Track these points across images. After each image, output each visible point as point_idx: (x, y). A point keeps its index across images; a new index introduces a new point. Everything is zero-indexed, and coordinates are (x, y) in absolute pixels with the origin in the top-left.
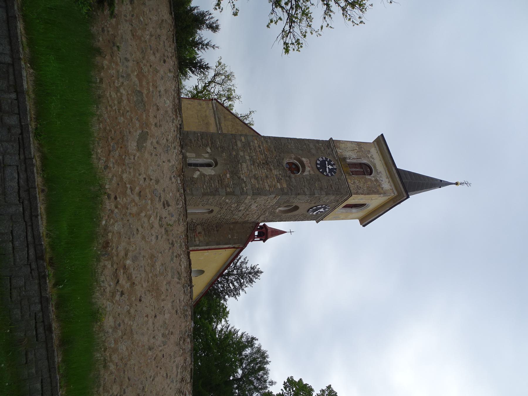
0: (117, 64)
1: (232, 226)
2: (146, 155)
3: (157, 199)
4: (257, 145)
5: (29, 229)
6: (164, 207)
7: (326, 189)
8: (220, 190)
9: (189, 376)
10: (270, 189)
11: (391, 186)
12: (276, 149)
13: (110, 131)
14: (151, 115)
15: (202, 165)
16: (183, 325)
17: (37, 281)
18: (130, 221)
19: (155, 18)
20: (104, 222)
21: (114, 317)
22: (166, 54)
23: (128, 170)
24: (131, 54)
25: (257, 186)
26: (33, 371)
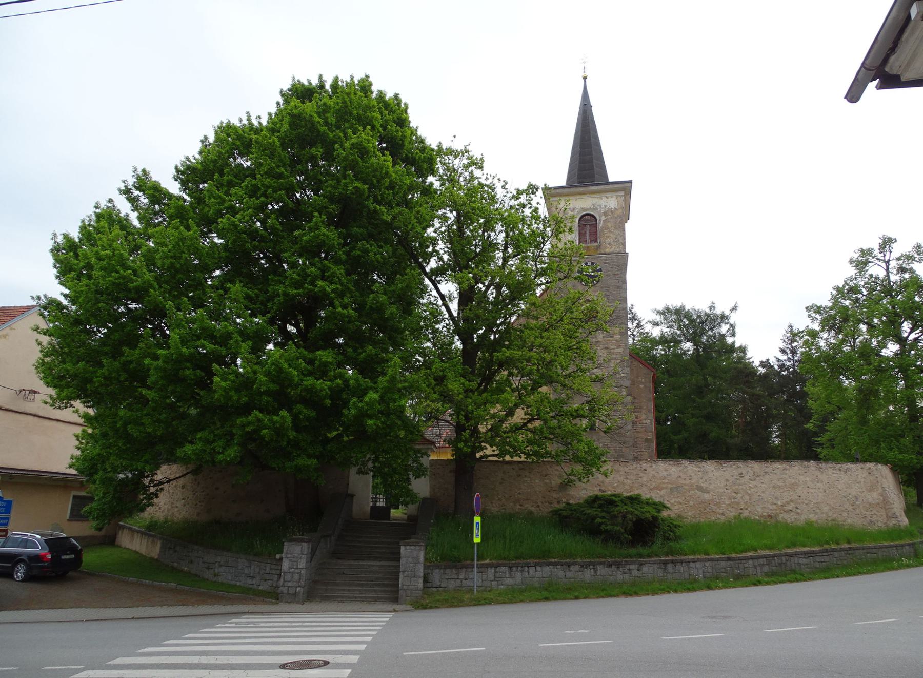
2: (711, 487)
3: (738, 481)
7: (619, 282)
11: (612, 197)
13: (700, 510)
14: (684, 482)
16: (813, 468)
20: (757, 517)
22: (639, 468)
23: (723, 500)
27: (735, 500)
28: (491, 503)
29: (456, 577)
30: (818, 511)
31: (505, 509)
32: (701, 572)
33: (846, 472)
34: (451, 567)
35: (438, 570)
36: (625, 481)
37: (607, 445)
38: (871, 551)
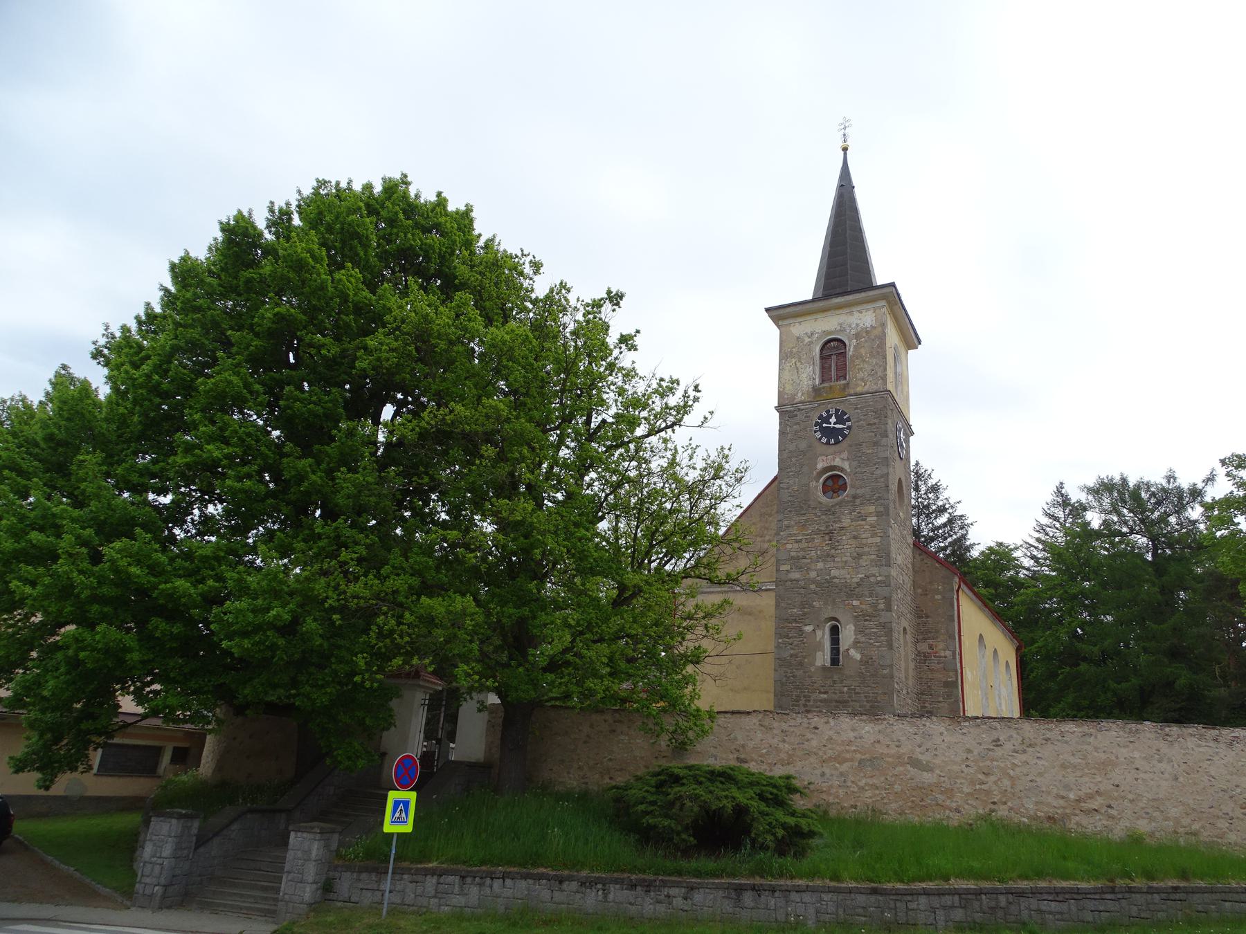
0: (831, 787)
1: (919, 591)
2: (937, 761)
4: (796, 545)
5: (1088, 896)
6: (1001, 745)
8: (882, 620)
9: (1212, 731)
10: (879, 534)
11: (867, 310)
12: (803, 512)
13: (913, 802)
14: (886, 751)
15: (835, 641)
16: (1148, 735)
17: (1133, 895)
18: (1021, 789)
19: (759, 735)
21: (1138, 819)
23: (958, 785)
24: (815, 768)
25: (873, 557)
26: (1213, 907)
27: (983, 786)
28: (569, 773)
29: (375, 887)
30: (1157, 814)
31: (587, 783)
32: (812, 911)
33: (1231, 744)
34: (368, 870)
35: (349, 873)
36: (781, 745)
37: (855, 689)
38: (1230, 897)
